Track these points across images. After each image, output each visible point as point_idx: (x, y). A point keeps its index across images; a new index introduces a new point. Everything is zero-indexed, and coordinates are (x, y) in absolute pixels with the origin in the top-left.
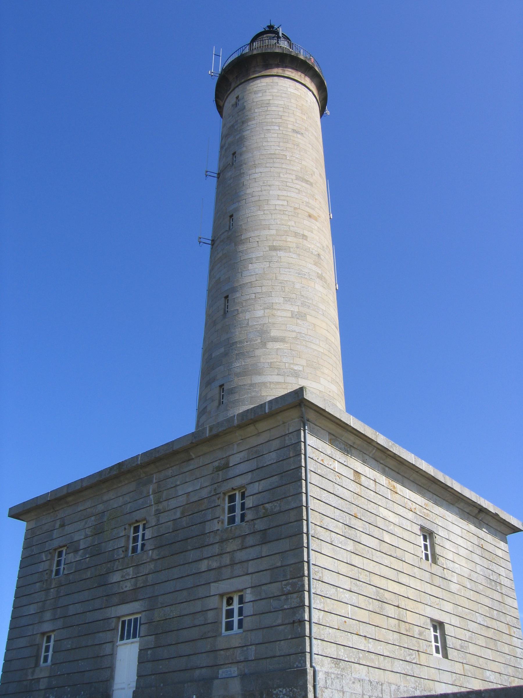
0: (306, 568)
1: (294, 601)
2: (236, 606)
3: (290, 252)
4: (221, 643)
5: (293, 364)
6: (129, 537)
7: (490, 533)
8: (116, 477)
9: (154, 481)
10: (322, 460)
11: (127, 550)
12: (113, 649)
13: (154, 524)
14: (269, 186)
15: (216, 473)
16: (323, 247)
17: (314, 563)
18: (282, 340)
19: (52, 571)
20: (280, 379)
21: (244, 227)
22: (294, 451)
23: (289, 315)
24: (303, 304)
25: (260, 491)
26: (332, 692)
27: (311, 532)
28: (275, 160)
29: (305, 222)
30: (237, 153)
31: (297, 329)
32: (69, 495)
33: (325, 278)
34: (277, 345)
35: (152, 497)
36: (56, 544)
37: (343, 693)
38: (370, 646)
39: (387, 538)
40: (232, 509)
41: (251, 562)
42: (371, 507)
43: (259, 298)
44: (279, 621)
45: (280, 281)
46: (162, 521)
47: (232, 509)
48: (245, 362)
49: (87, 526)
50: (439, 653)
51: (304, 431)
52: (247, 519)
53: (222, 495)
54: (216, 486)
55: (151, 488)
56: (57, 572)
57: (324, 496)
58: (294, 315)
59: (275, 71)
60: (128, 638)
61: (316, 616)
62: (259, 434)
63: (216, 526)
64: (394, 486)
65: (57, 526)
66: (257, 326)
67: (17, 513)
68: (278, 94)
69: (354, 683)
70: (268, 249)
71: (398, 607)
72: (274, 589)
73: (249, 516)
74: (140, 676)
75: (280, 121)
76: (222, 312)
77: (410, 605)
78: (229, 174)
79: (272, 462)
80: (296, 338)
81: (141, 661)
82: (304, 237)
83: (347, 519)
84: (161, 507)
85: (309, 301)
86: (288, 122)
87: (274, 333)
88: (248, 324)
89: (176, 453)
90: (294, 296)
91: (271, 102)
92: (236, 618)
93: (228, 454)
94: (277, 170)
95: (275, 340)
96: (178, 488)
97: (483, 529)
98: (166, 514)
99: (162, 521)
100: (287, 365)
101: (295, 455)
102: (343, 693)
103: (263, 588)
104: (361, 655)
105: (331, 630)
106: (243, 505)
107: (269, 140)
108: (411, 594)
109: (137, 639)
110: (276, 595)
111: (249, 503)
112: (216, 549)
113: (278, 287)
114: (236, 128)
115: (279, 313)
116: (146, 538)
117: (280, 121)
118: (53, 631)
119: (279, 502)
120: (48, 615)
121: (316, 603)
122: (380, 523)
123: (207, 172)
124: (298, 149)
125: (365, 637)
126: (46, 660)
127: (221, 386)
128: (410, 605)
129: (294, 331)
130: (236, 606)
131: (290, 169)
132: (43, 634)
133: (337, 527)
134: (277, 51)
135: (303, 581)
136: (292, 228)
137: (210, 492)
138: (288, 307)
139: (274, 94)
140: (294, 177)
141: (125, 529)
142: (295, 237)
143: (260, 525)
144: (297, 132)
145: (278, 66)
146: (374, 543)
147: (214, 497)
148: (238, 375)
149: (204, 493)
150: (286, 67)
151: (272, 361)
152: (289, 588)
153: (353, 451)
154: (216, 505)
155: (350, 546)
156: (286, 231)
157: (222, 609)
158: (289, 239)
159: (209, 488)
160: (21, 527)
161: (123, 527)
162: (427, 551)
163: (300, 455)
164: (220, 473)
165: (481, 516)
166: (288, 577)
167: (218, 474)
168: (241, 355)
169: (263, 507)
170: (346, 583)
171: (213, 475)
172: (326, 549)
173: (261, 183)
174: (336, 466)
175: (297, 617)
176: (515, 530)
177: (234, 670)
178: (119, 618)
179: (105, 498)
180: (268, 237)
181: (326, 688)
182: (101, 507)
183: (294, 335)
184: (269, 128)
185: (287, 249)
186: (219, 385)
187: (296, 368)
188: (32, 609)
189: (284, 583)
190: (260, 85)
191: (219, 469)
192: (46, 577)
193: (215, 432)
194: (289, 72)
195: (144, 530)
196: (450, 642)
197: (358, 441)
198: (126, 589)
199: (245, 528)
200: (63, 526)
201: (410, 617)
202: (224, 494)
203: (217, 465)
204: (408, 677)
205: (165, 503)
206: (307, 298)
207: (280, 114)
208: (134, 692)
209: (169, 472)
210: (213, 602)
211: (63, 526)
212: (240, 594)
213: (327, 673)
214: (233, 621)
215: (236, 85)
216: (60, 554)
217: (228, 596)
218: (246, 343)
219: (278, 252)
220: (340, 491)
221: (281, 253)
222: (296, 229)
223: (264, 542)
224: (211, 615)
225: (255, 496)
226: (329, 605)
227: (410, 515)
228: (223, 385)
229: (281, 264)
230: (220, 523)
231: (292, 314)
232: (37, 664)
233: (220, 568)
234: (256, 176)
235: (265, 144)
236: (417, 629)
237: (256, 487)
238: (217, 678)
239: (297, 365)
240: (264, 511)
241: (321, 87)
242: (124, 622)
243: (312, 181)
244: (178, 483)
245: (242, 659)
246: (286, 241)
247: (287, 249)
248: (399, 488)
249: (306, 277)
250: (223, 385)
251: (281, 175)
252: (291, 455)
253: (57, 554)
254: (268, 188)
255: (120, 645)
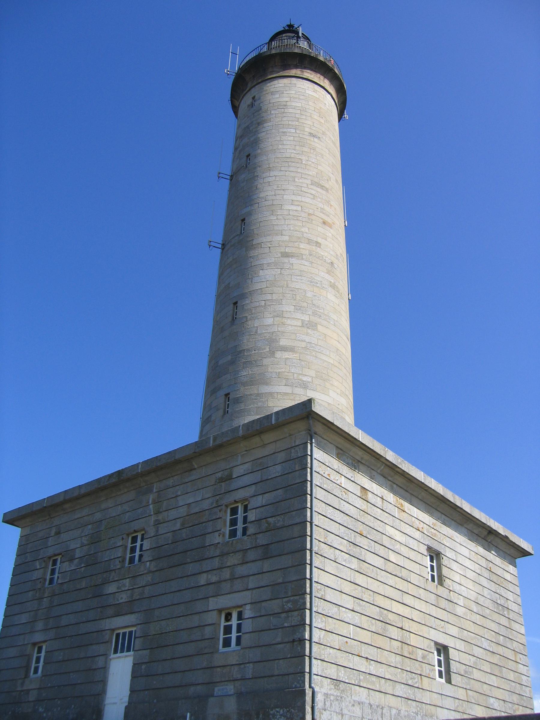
0: (308, 585)
1: (294, 619)
2: (234, 622)
3: (302, 259)
4: (218, 660)
5: (302, 374)
6: (126, 547)
7: (499, 556)
8: (115, 485)
9: (155, 490)
10: (329, 475)
11: (124, 561)
12: (106, 662)
13: (152, 535)
14: (283, 190)
15: (219, 484)
16: (337, 255)
17: (317, 581)
18: (291, 349)
19: (45, 580)
20: (288, 390)
21: (256, 232)
22: (300, 465)
23: (299, 323)
24: (315, 313)
25: (264, 504)
26: (331, 714)
27: (315, 549)
28: (290, 163)
29: (320, 229)
30: (251, 155)
31: (307, 339)
32: (65, 502)
33: (337, 288)
34: (286, 355)
35: (151, 506)
36: (50, 551)
37: (342, 715)
38: (372, 668)
39: (393, 557)
40: (234, 522)
41: (251, 578)
42: (377, 525)
43: (269, 305)
44: (279, 640)
45: (291, 289)
46: (161, 531)
47: (234, 522)
48: (252, 371)
49: (83, 534)
50: (442, 678)
51: (311, 444)
52: (248, 533)
53: (223, 507)
54: (218, 497)
55: (151, 497)
56: (51, 581)
57: (330, 512)
58: (304, 325)
59: (293, 72)
60: (122, 651)
61: (317, 635)
62: (264, 446)
63: (217, 539)
64: (402, 504)
65: (53, 533)
66: (265, 335)
67: (11, 519)
68: (295, 96)
69: (353, 705)
70: (280, 255)
71: (401, 628)
72: (275, 605)
73: (251, 530)
74: (132, 691)
75: (297, 123)
76: (230, 319)
77: (414, 627)
78: (243, 176)
79: (277, 475)
80: (306, 348)
81: (135, 675)
82: (318, 244)
83: (352, 537)
84: (160, 517)
85: (320, 311)
86: (305, 125)
87: (283, 342)
88: (256, 332)
89: (178, 462)
90: (305, 304)
91: (288, 104)
92: (234, 635)
93: (231, 465)
94: (293, 174)
95: (284, 349)
96: (179, 498)
97: (492, 552)
98: (165, 525)
99: (161, 531)
100: (295, 375)
101: (300, 468)
102: (342, 715)
103: (264, 604)
104: (362, 677)
105: (332, 650)
106: (245, 518)
107: (285, 143)
108: (415, 615)
109: (132, 653)
110: (276, 612)
111: (252, 516)
112: (216, 562)
113: (289, 295)
114: (251, 128)
115: (289, 322)
116: (144, 549)
117: (297, 123)
118: (45, 642)
119: (282, 517)
120: (40, 625)
121: (318, 622)
122: (386, 541)
123: (219, 173)
124: (315, 153)
125: (367, 658)
126: (36, 671)
127: (227, 395)
128: (414, 627)
129: (304, 341)
130: (234, 622)
131: (306, 174)
132: (34, 644)
133: (341, 544)
134: (296, 51)
135: (305, 599)
136: (305, 235)
137: (212, 503)
138: (298, 315)
139: (291, 96)
140: (309, 182)
141: (123, 539)
142: (308, 243)
143: (262, 540)
144: (314, 136)
145: (296, 67)
146: (378, 562)
147: (216, 509)
148: (244, 384)
149: (206, 505)
150: (305, 68)
151: (280, 371)
152: (289, 605)
153: (361, 466)
154: (218, 517)
155: (355, 564)
156: (299, 238)
157: (220, 625)
158: (302, 246)
159: (210, 500)
160: (14, 534)
161: (121, 537)
162: (434, 572)
163: (306, 468)
164: (223, 484)
165: (491, 538)
166: (290, 594)
167: (221, 486)
168: (248, 364)
169: (266, 521)
170: (349, 603)
171: (215, 486)
172: (330, 567)
173: (275, 187)
174: (343, 481)
175: (297, 636)
176: (525, 553)
177: (230, 688)
178: (113, 630)
179: (103, 506)
180: (280, 243)
181: (325, 710)
182: (98, 516)
183: (303, 345)
184: (285, 130)
185: (300, 256)
186: (225, 393)
187: (305, 379)
188: (24, 618)
189: (285, 600)
190: (277, 86)
191: (221, 480)
192: (39, 586)
193: (218, 442)
194: (308, 74)
195: (142, 540)
196: (454, 667)
197: (367, 457)
198: (121, 601)
199: (247, 542)
200: (58, 533)
201: (413, 640)
202: (227, 506)
203: (220, 476)
204: (410, 702)
205: (165, 514)
206: (318, 307)
207: (297, 116)
208: (126, 707)
209: (170, 482)
210: (211, 618)
211: (58, 533)
212: (239, 610)
213: (326, 695)
214: (231, 637)
215: (253, 85)
216: (55, 562)
217: (227, 611)
218: (254, 352)
219: (290, 259)
220: (346, 507)
221: (293, 260)
222: (310, 235)
223: (266, 557)
224: (208, 631)
225: (258, 510)
226: (331, 625)
227: (417, 535)
228: (229, 394)
229: (293, 271)
230: (221, 536)
231: (302, 324)
232: (27, 675)
233: (220, 582)
234: (270, 179)
235: (280, 147)
236: (420, 652)
237: (259, 501)
238: (213, 696)
239: (306, 375)
240: (267, 525)
241: (341, 90)
242: (118, 635)
243: (327, 186)
244: (179, 493)
245: (239, 676)
246: (299, 248)
247: (300, 256)
248: (407, 506)
249: (318, 285)
250: (229, 394)
251: (296, 180)
252: (297, 468)
253: (51, 563)
254: (282, 192)
255: (114, 658)
